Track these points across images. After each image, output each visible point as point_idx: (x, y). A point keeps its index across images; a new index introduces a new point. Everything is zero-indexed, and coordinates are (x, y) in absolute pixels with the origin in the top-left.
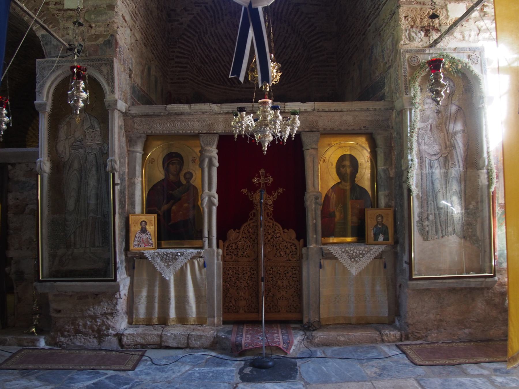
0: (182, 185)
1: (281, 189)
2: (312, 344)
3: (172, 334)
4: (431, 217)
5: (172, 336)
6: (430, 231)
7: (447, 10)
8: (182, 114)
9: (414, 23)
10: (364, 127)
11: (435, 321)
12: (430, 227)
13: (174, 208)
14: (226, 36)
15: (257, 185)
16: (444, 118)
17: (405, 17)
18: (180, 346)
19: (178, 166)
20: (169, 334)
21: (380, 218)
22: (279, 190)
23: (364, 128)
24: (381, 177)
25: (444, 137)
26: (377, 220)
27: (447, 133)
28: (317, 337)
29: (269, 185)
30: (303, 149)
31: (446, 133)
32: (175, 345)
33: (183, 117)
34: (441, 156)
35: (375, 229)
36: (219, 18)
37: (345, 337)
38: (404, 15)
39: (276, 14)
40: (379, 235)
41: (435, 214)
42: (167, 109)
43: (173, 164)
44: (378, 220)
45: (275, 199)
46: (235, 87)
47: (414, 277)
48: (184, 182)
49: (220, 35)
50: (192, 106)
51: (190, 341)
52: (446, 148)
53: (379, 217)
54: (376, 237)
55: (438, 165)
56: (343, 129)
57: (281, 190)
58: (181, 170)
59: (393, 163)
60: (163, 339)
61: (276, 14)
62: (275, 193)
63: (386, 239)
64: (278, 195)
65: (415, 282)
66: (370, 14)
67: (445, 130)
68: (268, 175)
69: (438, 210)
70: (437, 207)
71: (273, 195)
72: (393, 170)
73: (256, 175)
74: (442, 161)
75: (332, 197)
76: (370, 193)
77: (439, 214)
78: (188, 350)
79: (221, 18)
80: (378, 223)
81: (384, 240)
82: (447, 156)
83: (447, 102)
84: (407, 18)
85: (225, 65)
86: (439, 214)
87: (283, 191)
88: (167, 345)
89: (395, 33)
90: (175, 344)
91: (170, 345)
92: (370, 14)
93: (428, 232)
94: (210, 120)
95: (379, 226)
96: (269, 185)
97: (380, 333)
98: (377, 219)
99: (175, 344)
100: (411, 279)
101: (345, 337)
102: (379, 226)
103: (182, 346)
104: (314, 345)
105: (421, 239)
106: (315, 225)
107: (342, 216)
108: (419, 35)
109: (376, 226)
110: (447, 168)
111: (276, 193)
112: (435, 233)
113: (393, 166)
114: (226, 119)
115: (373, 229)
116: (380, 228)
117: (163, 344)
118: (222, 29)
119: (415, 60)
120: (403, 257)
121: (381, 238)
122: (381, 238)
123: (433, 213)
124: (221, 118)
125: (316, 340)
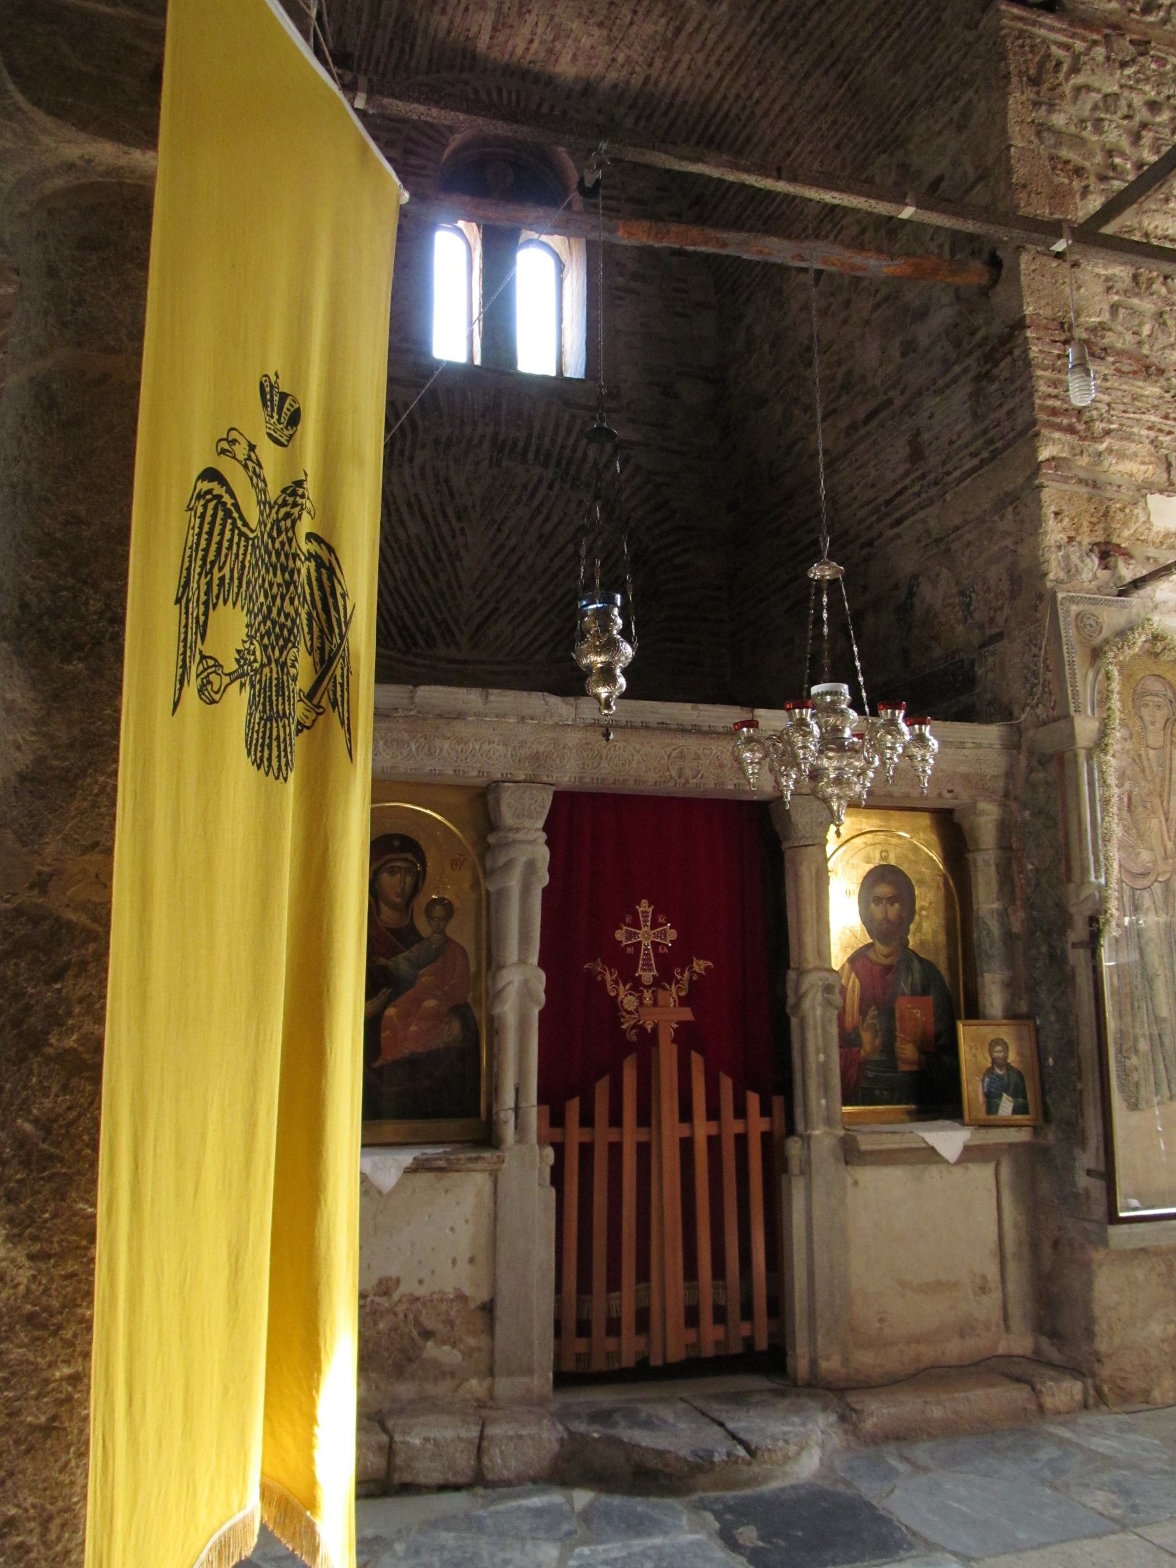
0: (419, 938)
1: (701, 962)
2: (858, 1438)
3: (427, 1440)
4: (1143, 1045)
5: (428, 1446)
6: (1142, 1083)
7: (1145, 508)
8: (460, 716)
9: (1076, 530)
10: (950, 791)
11: (1163, 1341)
12: (1141, 1071)
13: (391, 1011)
14: (410, 505)
15: (630, 950)
16: (1158, 780)
17: (1056, 514)
18: (451, 1478)
19: (409, 880)
20: (417, 1442)
21: (999, 1048)
22: (695, 965)
23: (950, 795)
24: (989, 932)
25: (1161, 829)
26: (991, 1055)
27: (1167, 820)
28: (872, 1414)
29: (666, 950)
30: (785, 846)
31: (1163, 819)
32: (437, 1478)
33: (459, 726)
34: (1156, 881)
35: (987, 1080)
36: (402, 452)
37: (944, 1407)
38: (1053, 508)
39: (564, 462)
40: (1000, 1097)
41: (1151, 1035)
42: (416, 700)
43: (392, 872)
44: (995, 1055)
45: (683, 994)
46: (416, 655)
47: (1122, 1215)
48: (423, 926)
49: (395, 503)
50: (492, 698)
51: (486, 1461)
52: (1166, 858)
53: (997, 1044)
54: (992, 1105)
55: (1151, 904)
56: (897, 794)
57: (700, 965)
58: (416, 890)
59: (1018, 893)
60: (399, 1461)
61: (564, 462)
62: (682, 974)
63: (1019, 1109)
64: (691, 981)
65: (1124, 1228)
66: (900, 493)
67: (1161, 811)
68: (661, 920)
69: (1156, 1023)
70: (1156, 1017)
71: (677, 982)
72: (1021, 914)
73: (628, 920)
74: (1159, 891)
75: (850, 987)
76: (947, 979)
77: (1160, 1035)
78: (480, 1491)
79: (407, 454)
80: (994, 1061)
81: (1015, 1111)
82: (1169, 879)
83: (1161, 739)
84: (1060, 517)
85: (396, 588)
86: (1160, 1035)
87: (707, 969)
88: (407, 1478)
89: (1022, 550)
90: (436, 1474)
91: (422, 1479)
92: (900, 493)
93: (1137, 1085)
94: (541, 743)
95: (999, 1072)
96: (666, 950)
97: (1033, 1389)
98: (991, 1052)
99: (436, 1474)
100: (1113, 1218)
101: (944, 1407)
102: (999, 1072)
103: (461, 1479)
104: (865, 1442)
105: (1124, 1105)
106: (824, 1067)
107: (877, 1041)
108: (1088, 561)
109: (990, 1071)
110: (1171, 912)
111: (686, 974)
112: (1153, 1088)
113: (1019, 903)
114: (587, 744)
115: (983, 1081)
116: (1000, 1078)
117: (397, 1478)
118: (405, 485)
119: (1091, 625)
120: (1074, 1159)
121: (1006, 1106)
122: (1006, 1106)
123: (1147, 1033)
124: (573, 738)
125: (869, 1425)
